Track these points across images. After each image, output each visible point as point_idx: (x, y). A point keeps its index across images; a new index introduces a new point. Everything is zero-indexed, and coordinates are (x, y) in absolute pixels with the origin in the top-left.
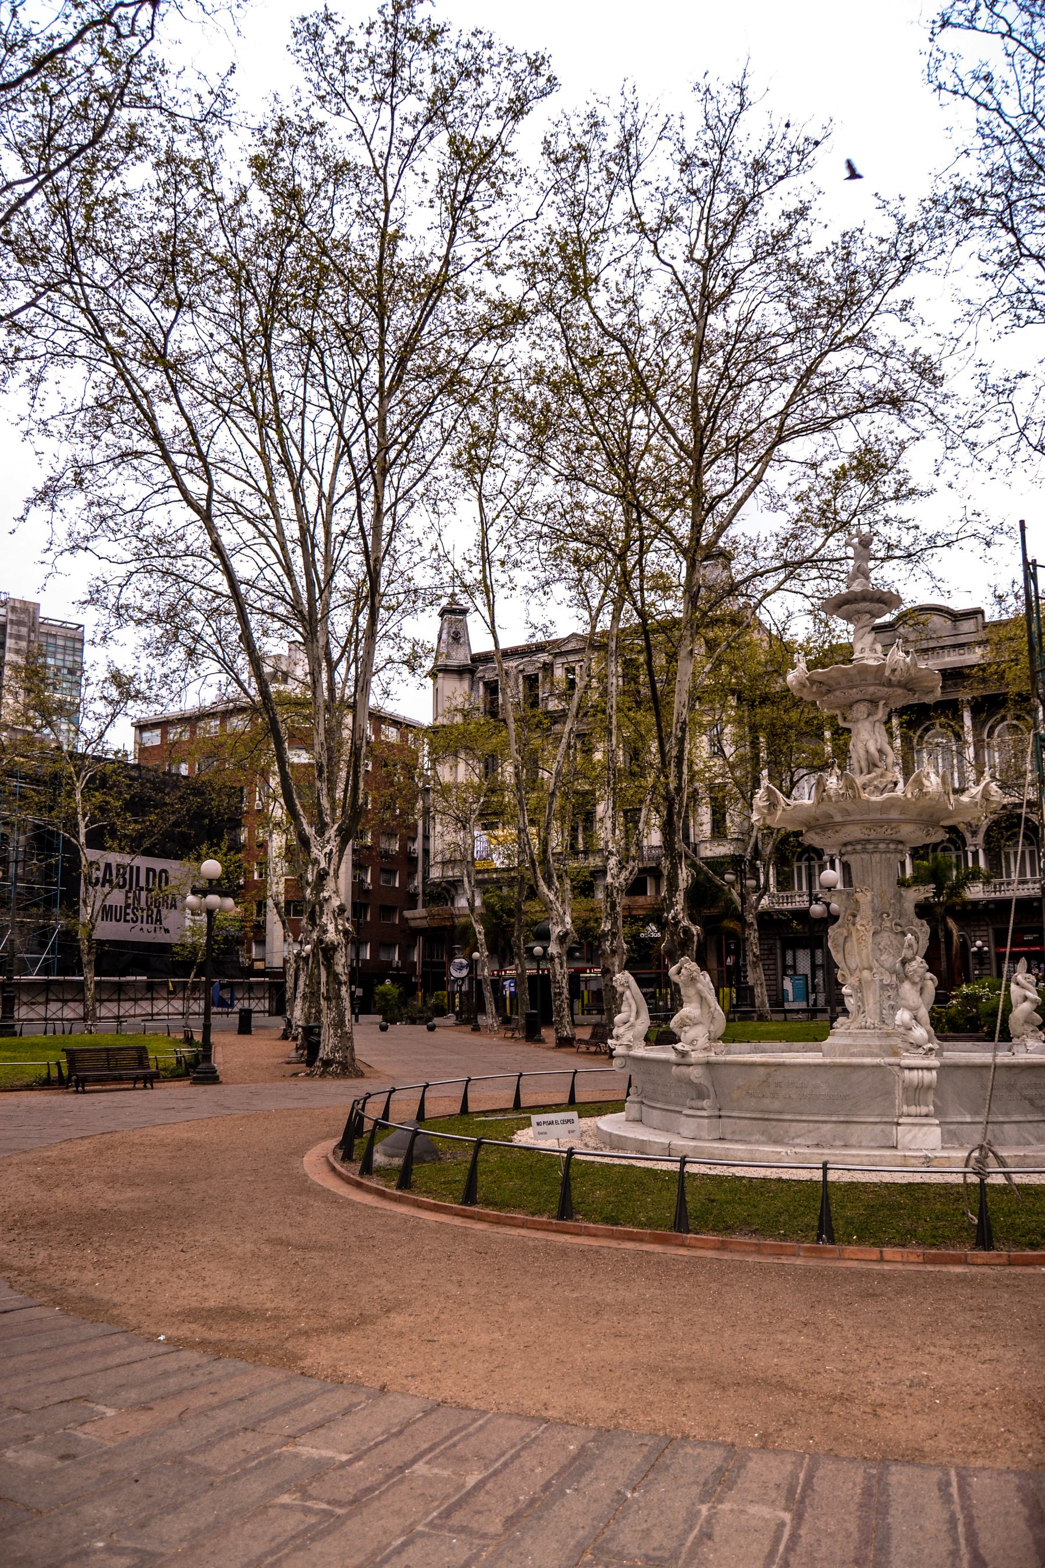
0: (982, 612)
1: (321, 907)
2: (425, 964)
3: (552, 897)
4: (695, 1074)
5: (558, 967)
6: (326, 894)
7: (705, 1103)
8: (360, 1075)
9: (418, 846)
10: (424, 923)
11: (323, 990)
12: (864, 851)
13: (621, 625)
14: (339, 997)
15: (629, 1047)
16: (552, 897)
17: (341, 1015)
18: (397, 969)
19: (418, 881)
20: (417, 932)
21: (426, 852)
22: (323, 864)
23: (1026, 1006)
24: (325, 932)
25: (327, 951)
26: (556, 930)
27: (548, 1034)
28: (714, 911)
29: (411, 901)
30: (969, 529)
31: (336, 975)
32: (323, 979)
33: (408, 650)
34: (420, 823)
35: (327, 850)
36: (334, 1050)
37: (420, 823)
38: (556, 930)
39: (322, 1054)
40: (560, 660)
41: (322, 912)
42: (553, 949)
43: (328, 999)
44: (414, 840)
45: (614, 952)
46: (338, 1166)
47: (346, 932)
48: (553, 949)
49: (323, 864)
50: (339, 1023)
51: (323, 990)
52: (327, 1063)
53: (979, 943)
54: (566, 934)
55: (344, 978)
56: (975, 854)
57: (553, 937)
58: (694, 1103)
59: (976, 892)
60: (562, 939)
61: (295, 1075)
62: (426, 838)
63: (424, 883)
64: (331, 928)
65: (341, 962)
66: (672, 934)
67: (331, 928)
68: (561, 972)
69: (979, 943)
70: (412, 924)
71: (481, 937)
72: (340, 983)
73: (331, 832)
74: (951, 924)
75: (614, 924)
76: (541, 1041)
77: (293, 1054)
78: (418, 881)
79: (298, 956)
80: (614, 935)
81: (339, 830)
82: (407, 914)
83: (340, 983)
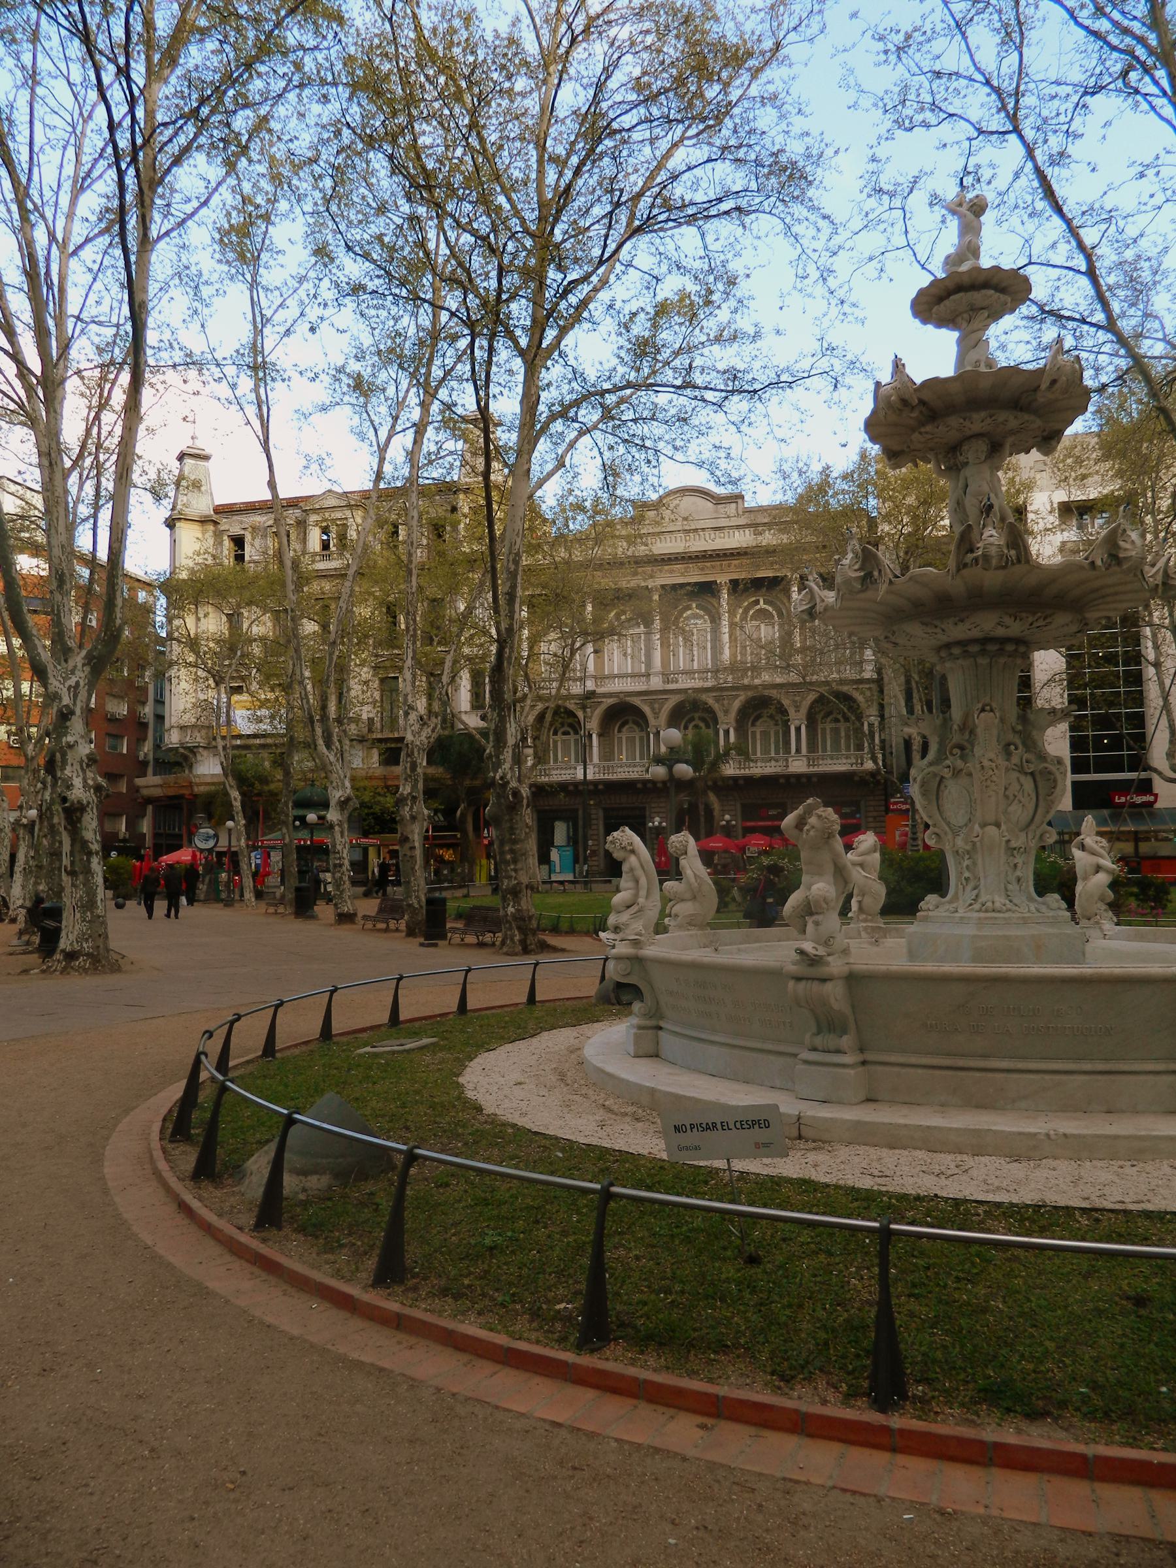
0: (742, 497)
1: (64, 755)
2: (156, 835)
3: (332, 758)
4: (834, 992)
5: (338, 836)
6: (70, 739)
7: (846, 1041)
8: (116, 968)
9: (148, 710)
10: (158, 792)
11: (66, 861)
12: (983, 652)
13: (382, 486)
14: (88, 871)
15: (636, 943)
16: (332, 758)
17: (91, 894)
18: (124, 840)
19: (147, 747)
20: (149, 800)
21: (160, 718)
22: (66, 700)
23: (1103, 878)
24: (69, 787)
25: (74, 813)
26: (336, 795)
27: (323, 910)
28: (477, 783)
29: (142, 767)
30: (823, 364)
31: (85, 843)
32: (66, 847)
33: (153, 475)
34: (151, 688)
35: (72, 681)
36: (82, 938)
37: (151, 688)
38: (336, 795)
39: (64, 944)
40: (313, 518)
41: (64, 762)
42: (333, 815)
43: (72, 873)
44: (144, 703)
45: (413, 818)
46: (188, 1198)
47: (98, 788)
48: (333, 815)
49: (66, 700)
50: (89, 904)
51: (66, 861)
52: (71, 956)
53: (727, 817)
54: (348, 799)
55: (95, 847)
56: (727, 732)
57: (333, 803)
58: (818, 1041)
59: (730, 769)
60: (343, 804)
61: (25, 972)
62: (160, 702)
63: (157, 747)
64: (77, 782)
65: (90, 826)
66: (499, 796)
67: (77, 782)
68: (343, 843)
69: (727, 817)
70: (145, 792)
71: (237, 804)
72: (90, 854)
73: (78, 659)
74: (712, 797)
75: (414, 787)
76: (313, 917)
77: (15, 942)
78: (147, 747)
79: (17, 822)
80: (414, 798)
81: (89, 658)
82: (139, 782)
83: (90, 854)
